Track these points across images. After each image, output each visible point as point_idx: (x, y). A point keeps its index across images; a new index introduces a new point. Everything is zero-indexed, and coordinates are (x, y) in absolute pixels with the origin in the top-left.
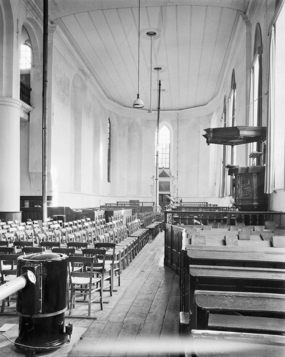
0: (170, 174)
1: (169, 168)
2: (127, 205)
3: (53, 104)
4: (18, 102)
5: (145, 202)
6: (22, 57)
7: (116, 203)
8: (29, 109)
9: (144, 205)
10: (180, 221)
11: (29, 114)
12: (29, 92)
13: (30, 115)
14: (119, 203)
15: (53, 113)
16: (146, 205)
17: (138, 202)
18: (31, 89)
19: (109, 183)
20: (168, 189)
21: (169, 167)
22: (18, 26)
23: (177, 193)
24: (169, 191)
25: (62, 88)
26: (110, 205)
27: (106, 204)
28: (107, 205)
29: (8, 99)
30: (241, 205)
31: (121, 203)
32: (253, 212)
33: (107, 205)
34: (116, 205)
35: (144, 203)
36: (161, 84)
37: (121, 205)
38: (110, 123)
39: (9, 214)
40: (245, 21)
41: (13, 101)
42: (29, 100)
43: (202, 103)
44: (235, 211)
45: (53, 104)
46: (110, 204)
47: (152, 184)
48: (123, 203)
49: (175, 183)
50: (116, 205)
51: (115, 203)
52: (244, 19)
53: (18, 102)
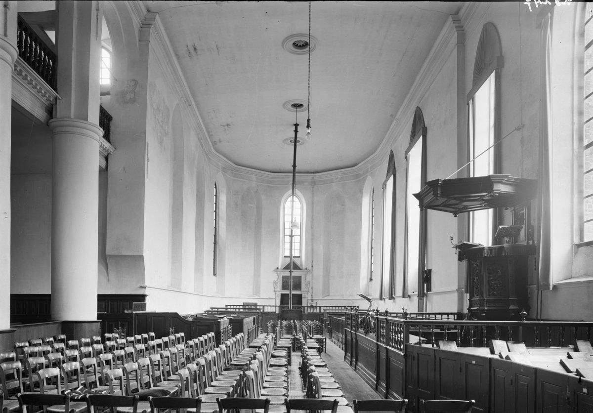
0: (302, 265)
1: (299, 257)
2: (232, 310)
3: (148, 144)
4: (95, 129)
5: (267, 306)
6: (103, 67)
7: (225, 307)
8: (108, 149)
9: (265, 311)
10: (433, 340)
11: (107, 158)
12: (109, 122)
13: (109, 159)
14: (229, 307)
15: (148, 158)
16: (269, 311)
17: (256, 305)
18: (112, 117)
19: (214, 277)
20: (298, 286)
21: (299, 255)
22: (97, 25)
23: (312, 293)
24: (301, 290)
25: (160, 121)
26: (217, 310)
27: (212, 308)
28: (213, 310)
29: (81, 123)
30: (486, 310)
31: (235, 307)
32: (505, 321)
33: (213, 310)
34: (224, 310)
35: (265, 308)
36: (294, 133)
37: (234, 310)
38: (216, 188)
39: (79, 324)
40: (457, 25)
41: (89, 126)
42: (108, 135)
43: (349, 163)
44: (429, 319)
45: (148, 144)
46: (218, 308)
47: (276, 280)
48: (238, 307)
49: (309, 278)
50: (224, 310)
51: (223, 307)
52: (454, 21)
53: (95, 129)
